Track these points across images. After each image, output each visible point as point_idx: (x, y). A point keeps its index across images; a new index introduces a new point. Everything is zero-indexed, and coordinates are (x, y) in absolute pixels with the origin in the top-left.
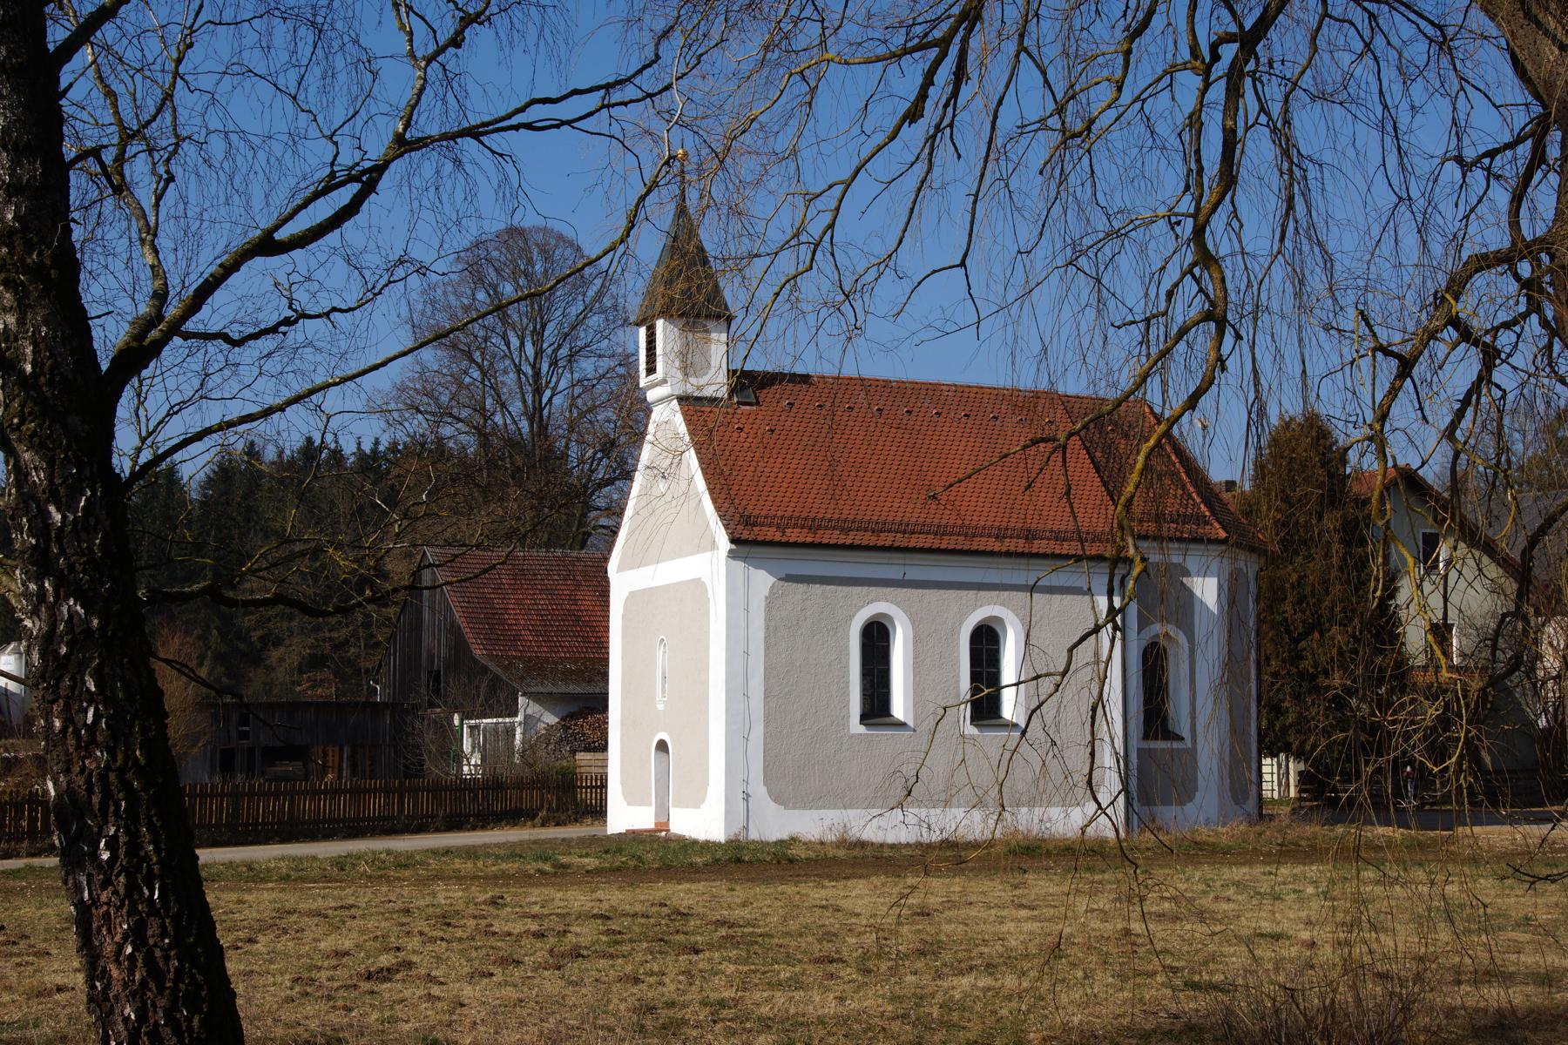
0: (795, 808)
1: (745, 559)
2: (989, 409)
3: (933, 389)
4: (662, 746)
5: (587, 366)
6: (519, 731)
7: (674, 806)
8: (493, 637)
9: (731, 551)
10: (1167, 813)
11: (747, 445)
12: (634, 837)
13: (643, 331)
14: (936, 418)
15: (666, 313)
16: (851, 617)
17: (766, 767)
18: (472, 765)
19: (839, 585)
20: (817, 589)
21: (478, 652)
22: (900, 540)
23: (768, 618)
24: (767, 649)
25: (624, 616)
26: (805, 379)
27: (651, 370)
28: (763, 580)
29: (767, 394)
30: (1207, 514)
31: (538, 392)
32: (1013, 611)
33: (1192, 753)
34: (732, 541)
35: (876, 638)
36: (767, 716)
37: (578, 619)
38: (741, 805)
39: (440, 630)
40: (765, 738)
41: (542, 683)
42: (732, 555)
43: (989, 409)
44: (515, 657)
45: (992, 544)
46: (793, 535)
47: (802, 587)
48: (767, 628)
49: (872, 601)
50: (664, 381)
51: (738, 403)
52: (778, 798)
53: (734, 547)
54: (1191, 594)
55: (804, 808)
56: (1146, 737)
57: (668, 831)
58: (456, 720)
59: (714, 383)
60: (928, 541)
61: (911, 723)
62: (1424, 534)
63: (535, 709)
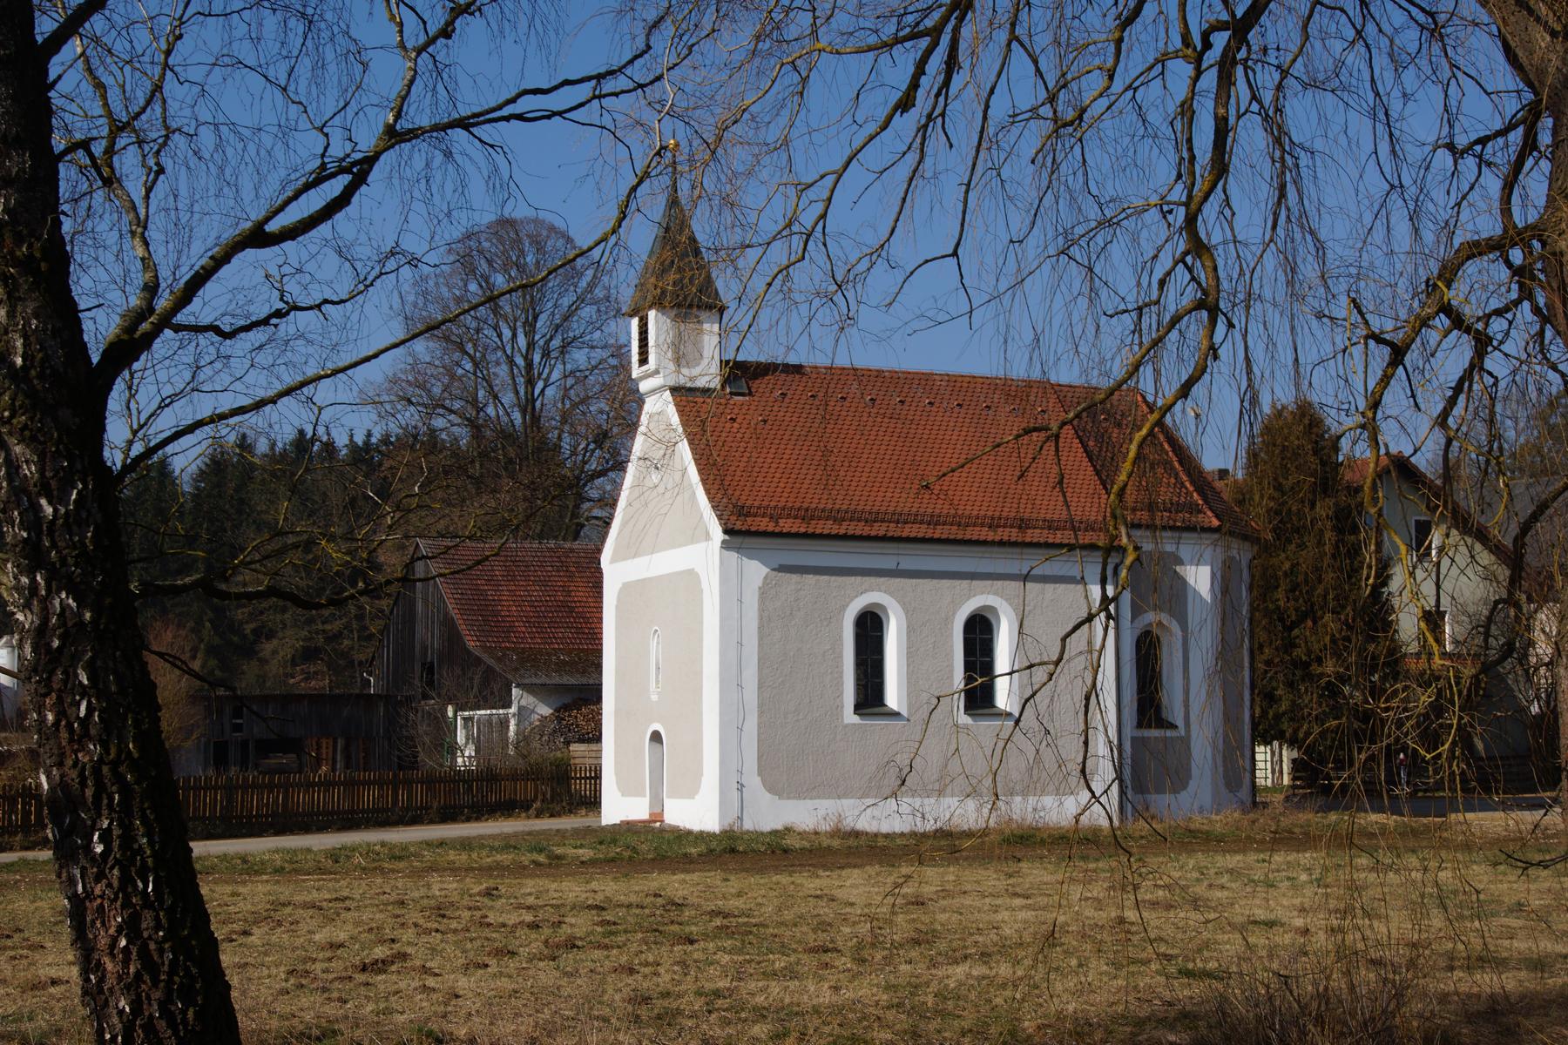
0: (789, 798)
1: (738, 549)
2: (982, 399)
3: (925, 379)
4: (656, 737)
5: (579, 357)
6: (513, 723)
7: (668, 797)
8: (487, 628)
9: (724, 542)
10: (1162, 802)
11: (739, 435)
12: (629, 827)
13: (635, 322)
14: (928, 408)
15: (659, 304)
16: (844, 607)
17: (760, 758)
18: (465, 759)
19: (832, 575)
20: (810, 579)
21: (471, 644)
22: (893, 530)
23: (762, 610)
24: (761, 638)
25: (617, 607)
26: (798, 369)
27: (643, 361)
28: (756, 571)
29: (760, 385)
30: (1200, 502)
31: (531, 383)
32: (1006, 600)
33: (1186, 741)
34: (726, 532)
35: (870, 628)
36: (761, 706)
37: (572, 610)
38: (736, 794)
39: (433, 622)
40: (759, 727)
41: (536, 675)
42: (725, 546)
43: (982, 399)
44: (508, 649)
45: (985, 534)
46: (786, 525)
47: (795, 577)
48: (761, 618)
49: (866, 591)
50: (657, 372)
51: (731, 393)
52: (772, 788)
53: (727, 537)
54: (1184, 582)
55: (799, 798)
56: (1140, 725)
57: (662, 821)
58: (450, 711)
59: (707, 373)
60: (922, 531)
61: (904, 713)
62: (1417, 522)
63: (528, 700)
